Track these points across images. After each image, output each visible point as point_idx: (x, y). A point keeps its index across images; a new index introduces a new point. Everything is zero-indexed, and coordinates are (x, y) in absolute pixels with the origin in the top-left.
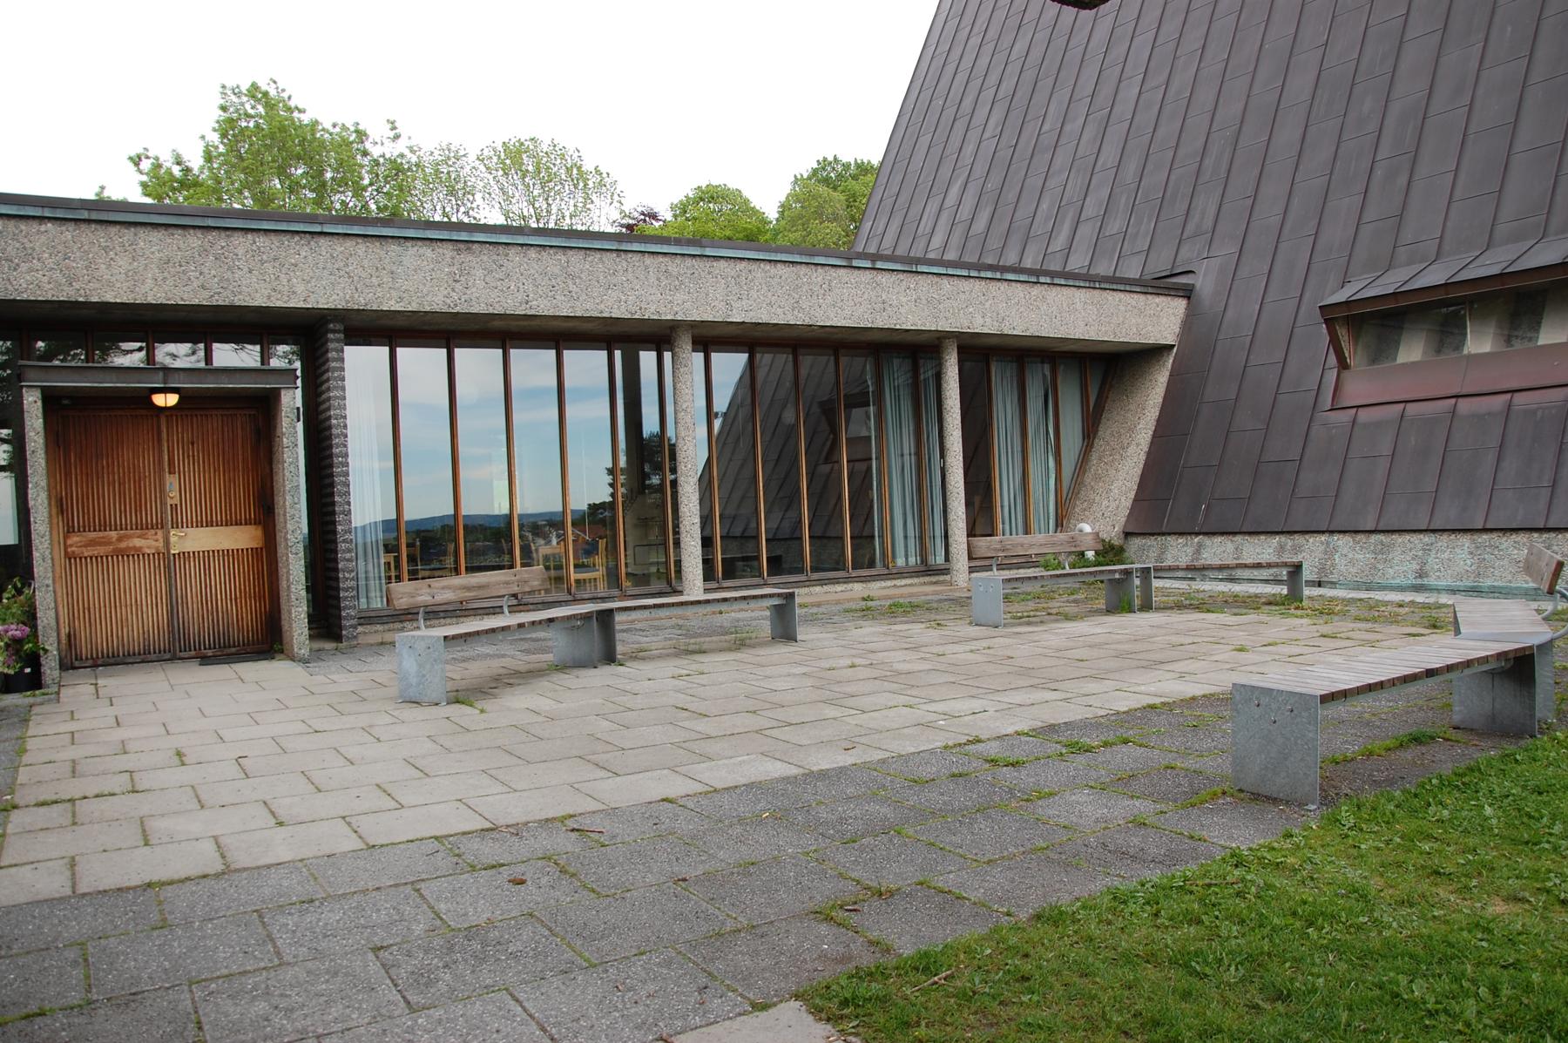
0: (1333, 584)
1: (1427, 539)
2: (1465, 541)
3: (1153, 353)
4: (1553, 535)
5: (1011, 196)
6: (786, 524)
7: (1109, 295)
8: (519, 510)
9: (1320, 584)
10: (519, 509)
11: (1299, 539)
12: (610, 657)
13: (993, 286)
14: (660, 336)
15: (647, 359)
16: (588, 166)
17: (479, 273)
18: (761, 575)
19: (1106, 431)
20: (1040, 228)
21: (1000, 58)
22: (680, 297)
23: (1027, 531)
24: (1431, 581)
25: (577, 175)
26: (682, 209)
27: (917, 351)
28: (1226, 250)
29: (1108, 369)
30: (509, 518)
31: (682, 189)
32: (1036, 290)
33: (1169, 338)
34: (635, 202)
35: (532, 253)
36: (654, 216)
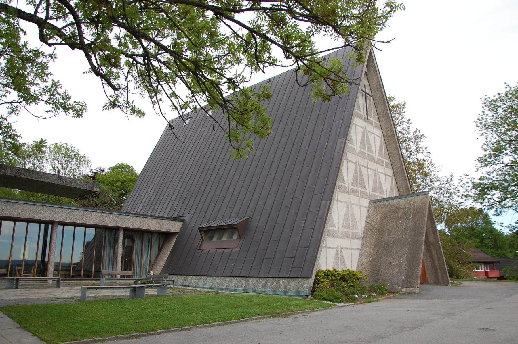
0: (191, 286)
1: (206, 277)
2: (211, 278)
3: (174, 234)
4: (233, 278)
5: (160, 192)
6: (88, 267)
7: (162, 221)
8: (62, 261)
9: (189, 286)
10: (62, 261)
11: (188, 277)
12: (17, 287)
13: (132, 218)
14: (53, 223)
15: (50, 226)
16: (81, 154)
17: (9, 208)
18: (69, 277)
19: (162, 251)
20: (163, 201)
21: (167, 156)
22: (55, 216)
23: (113, 270)
24: (205, 286)
25: (77, 157)
26: (113, 169)
27: (115, 230)
28: (192, 212)
29: (165, 236)
30: (8, 261)
31: (113, 163)
32: (143, 219)
33: (177, 230)
34: (95, 167)
35: (22, 205)
36: (103, 171)
